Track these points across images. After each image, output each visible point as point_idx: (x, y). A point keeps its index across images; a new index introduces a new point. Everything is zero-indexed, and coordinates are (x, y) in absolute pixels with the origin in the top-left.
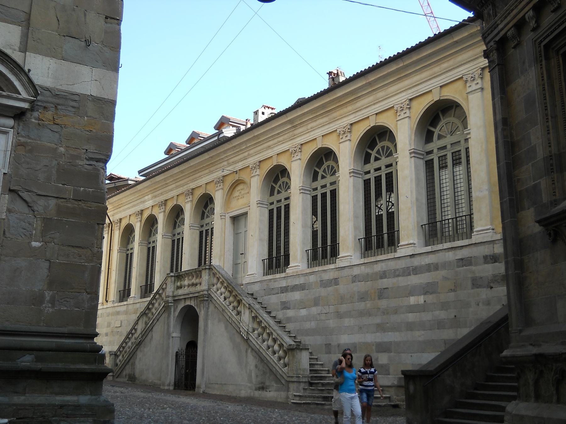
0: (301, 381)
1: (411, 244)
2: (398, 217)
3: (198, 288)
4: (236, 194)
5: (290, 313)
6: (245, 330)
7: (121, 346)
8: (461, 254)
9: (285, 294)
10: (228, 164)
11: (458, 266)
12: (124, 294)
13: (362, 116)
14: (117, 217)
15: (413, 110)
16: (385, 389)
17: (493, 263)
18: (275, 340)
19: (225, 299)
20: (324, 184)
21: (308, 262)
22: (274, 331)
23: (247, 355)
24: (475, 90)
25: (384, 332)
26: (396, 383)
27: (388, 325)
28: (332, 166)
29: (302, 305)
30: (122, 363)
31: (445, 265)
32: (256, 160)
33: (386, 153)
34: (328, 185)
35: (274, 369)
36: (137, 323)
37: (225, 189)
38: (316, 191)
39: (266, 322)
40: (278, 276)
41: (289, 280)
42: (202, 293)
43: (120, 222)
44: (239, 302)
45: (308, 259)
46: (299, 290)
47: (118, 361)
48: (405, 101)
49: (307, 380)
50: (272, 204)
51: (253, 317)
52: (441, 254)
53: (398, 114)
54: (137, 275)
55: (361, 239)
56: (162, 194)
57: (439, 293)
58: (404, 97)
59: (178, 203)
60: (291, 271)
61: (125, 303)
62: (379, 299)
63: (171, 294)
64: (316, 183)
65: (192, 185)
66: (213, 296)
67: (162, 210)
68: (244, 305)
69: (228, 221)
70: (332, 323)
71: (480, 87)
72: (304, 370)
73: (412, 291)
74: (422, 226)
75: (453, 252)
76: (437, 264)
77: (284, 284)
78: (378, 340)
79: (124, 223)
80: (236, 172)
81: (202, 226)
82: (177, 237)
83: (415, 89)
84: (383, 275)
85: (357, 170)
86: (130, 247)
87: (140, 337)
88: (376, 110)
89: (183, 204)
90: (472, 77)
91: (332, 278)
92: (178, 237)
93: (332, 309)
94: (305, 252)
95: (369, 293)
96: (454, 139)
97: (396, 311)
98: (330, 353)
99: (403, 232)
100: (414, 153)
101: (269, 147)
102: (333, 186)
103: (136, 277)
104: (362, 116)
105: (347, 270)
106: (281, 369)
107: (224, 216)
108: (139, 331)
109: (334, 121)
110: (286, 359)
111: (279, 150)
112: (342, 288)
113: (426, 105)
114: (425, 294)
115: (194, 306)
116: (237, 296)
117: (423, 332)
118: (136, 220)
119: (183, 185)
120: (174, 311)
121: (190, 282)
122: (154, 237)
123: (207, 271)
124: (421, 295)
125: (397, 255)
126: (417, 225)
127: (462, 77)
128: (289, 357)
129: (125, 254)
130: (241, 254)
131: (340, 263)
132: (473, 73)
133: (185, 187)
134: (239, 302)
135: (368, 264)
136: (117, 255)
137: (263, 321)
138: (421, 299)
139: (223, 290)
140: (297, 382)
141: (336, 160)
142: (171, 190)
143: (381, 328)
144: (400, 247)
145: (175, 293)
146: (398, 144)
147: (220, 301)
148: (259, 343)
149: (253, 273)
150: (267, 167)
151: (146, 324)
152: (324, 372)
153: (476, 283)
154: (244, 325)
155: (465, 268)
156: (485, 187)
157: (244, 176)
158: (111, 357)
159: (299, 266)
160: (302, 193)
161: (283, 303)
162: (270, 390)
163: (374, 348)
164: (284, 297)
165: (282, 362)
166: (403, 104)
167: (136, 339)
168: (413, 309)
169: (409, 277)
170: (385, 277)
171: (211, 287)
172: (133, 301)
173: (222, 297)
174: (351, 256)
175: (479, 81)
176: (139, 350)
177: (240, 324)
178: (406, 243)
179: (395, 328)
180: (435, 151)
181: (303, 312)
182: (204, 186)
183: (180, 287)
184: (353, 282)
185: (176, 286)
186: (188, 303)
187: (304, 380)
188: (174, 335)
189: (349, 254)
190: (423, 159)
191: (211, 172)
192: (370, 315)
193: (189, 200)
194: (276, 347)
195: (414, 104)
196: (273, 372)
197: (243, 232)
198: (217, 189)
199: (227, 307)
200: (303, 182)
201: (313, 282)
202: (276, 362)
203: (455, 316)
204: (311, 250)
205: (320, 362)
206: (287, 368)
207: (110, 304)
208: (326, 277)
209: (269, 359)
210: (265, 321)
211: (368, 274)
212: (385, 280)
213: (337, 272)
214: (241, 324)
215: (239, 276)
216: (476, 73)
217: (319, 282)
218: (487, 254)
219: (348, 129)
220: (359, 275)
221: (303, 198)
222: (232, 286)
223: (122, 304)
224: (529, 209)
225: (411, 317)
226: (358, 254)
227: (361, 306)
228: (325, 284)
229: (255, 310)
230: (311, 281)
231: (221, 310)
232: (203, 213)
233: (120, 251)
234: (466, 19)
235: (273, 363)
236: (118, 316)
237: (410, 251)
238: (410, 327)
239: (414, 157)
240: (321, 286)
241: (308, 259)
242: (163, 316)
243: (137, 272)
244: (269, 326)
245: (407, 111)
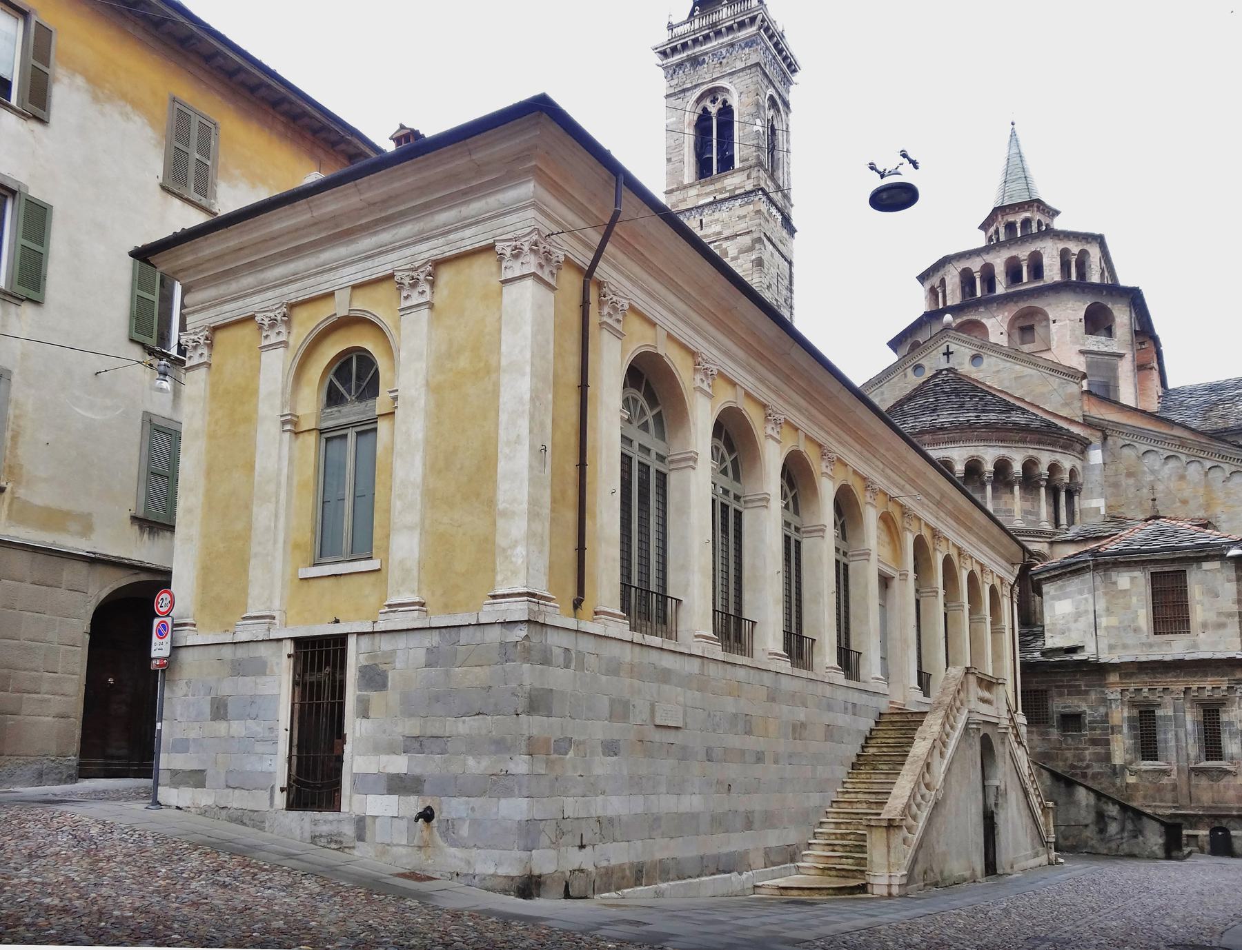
23: (1006, 786)
33: (358, 387)
90: (516, 248)
166: (199, 336)
195: (301, 315)
219: (282, 314)
234: (427, 135)
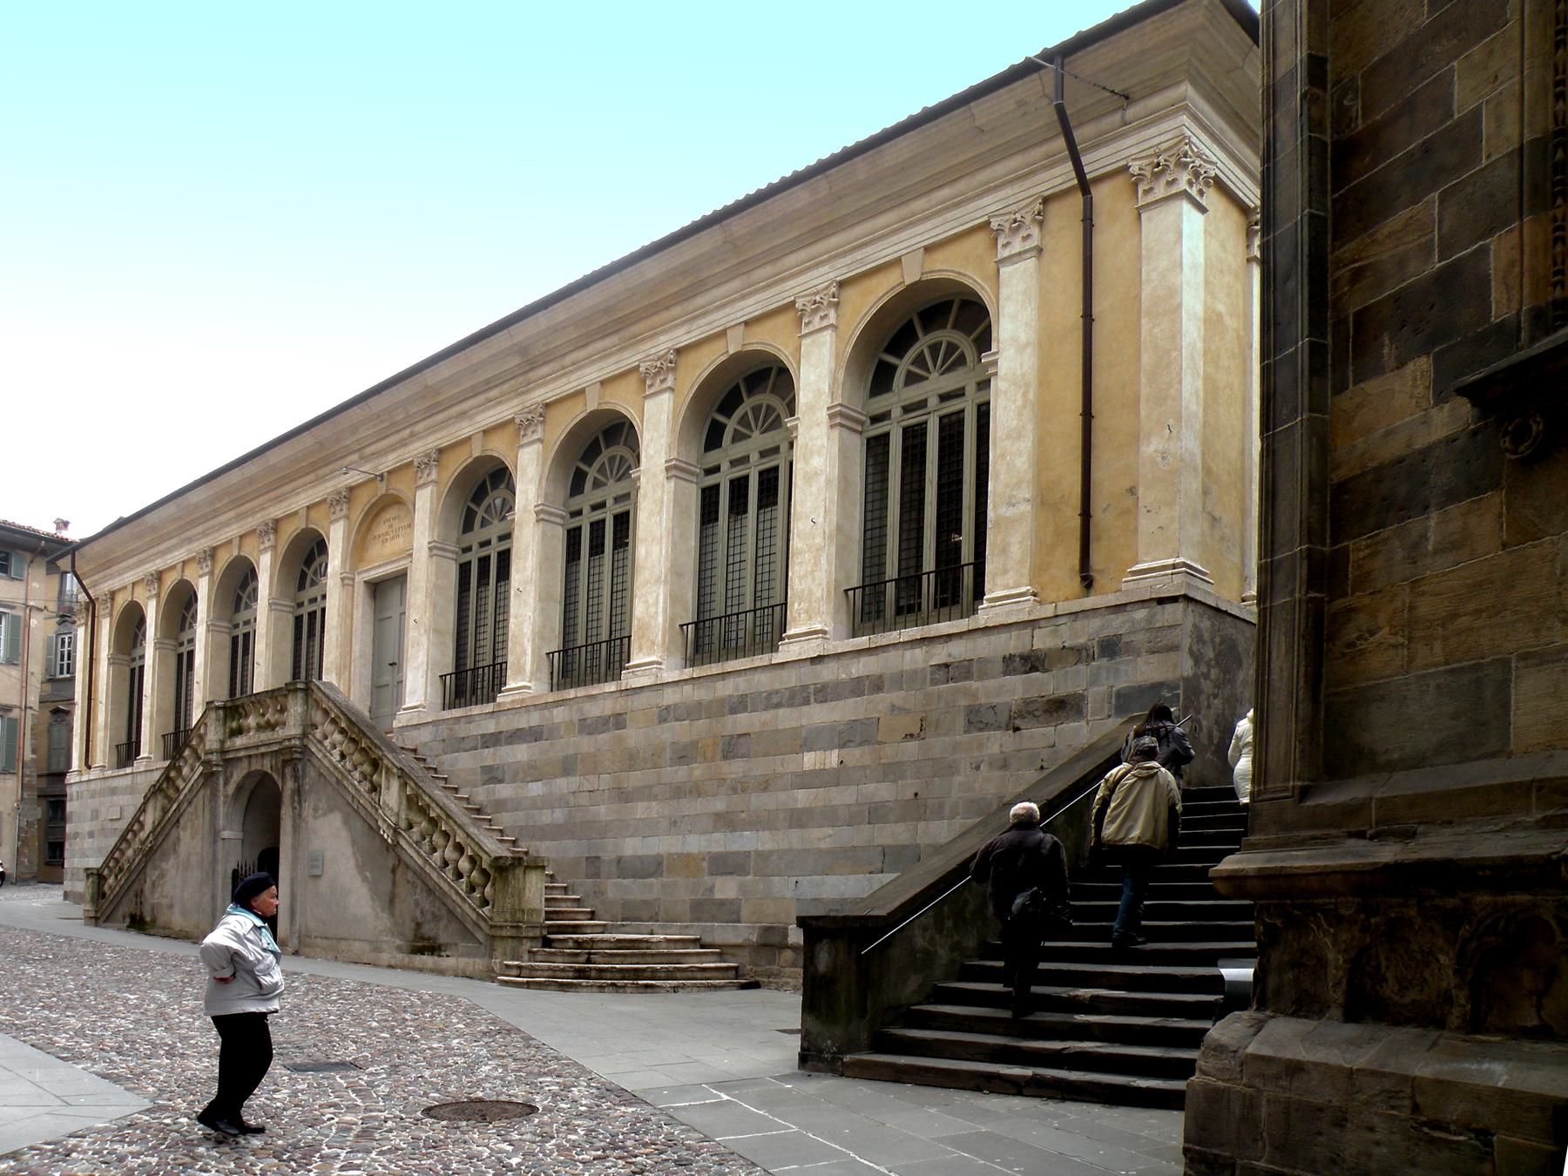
0: (524, 935)
1: (815, 632)
2: (784, 569)
3: (280, 733)
4: (381, 528)
5: (504, 791)
6: (389, 825)
7: (111, 855)
8: (941, 654)
9: (492, 750)
10: (362, 458)
11: (934, 682)
12: (128, 751)
13: (706, 328)
14: (107, 587)
15: (847, 309)
16: (725, 950)
17: (1026, 672)
18: (460, 849)
19: (343, 756)
20: (599, 500)
21: (552, 679)
22: (460, 826)
24: (1020, 254)
25: (734, 829)
26: (754, 938)
27: (743, 815)
28: (622, 457)
29: (533, 772)
30: (115, 892)
31: (901, 680)
32: (429, 446)
34: (610, 503)
35: (459, 910)
36: (144, 811)
37: (353, 517)
38: (577, 518)
39: (441, 808)
40: (476, 710)
41: (503, 719)
42: (287, 743)
43: (113, 599)
44: (376, 764)
45: (552, 673)
46: (525, 741)
47: (106, 888)
48: (827, 288)
49: (538, 934)
50: (467, 550)
51: (409, 798)
52: (892, 655)
53: (805, 320)
54: (152, 712)
55: (687, 625)
56: (205, 534)
57: (880, 743)
58: (824, 276)
59: (242, 554)
60: (509, 699)
61: (128, 770)
62: (725, 757)
63: (216, 746)
64: (579, 498)
65: (277, 512)
66: (313, 749)
67: (206, 570)
68: (388, 770)
69: (360, 591)
70: (603, 812)
71: (1036, 243)
72: (532, 911)
73: (809, 740)
74: (846, 591)
75: (924, 648)
76: (880, 677)
77: (490, 727)
78: (716, 849)
79: (121, 600)
80: (382, 476)
81: (300, 605)
82: (240, 632)
83: (858, 255)
84: (739, 704)
85: (686, 463)
86: (137, 653)
87: (151, 839)
88: (746, 311)
89: (255, 555)
90: (1015, 221)
91: (608, 712)
92: (246, 631)
93: (605, 781)
94: (545, 656)
95: (700, 745)
96: (950, 382)
97: (765, 786)
98: (597, 875)
99: (796, 605)
100: (840, 418)
101: (463, 415)
102: (622, 504)
103: (151, 717)
104: (706, 328)
105: (644, 696)
106: (475, 910)
107: (348, 578)
108: (148, 827)
109: (631, 345)
110: (488, 889)
111: (489, 421)
112: (634, 736)
113: (884, 295)
114: (842, 746)
115: (270, 772)
116: (370, 748)
117: (830, 831)
118: (148, 594)
119: (253, 512)
120: (226, 783)
121: (262, 721)
122: (192, 630)
123: (300, 695)
124: (832, 749)
125: (777, 658)
126: (836, 588)
127: (988, 223)
128: (493, 885)
129: (128, 671)
130: (391, 665)
131: (630, 680)
132: (1019, 210)
133: (259, 515)
134: (376, 764)
135: (702, 680)
136: (108, 670)
137: (433, 805)
138: (833, 758)
139: (337, 737)
140: (512, 937)
141: (634, 446)
142: (227, 524)
143: (724, 821)
144: (787, 641)
145: (228, 744)
146: (801, 393)
147: (330, 761)
148: (422, 853)
149: (417, 704)
150: (457, 463)
151: (165, 811)
152: (581, 917)
153: (977, 719)
154: (389, 813)
155: (951, 684)
156: (1026, 492)
157: (400, 486)
158: (91, 879)
159: (529, 688)
160: (542, 519)
161: (487, 769)
162: (448, 953)
163: (705, 864)
164: (489, 756)
165: (477, 895)
167: (143, 843)
168: (807, 780)
169: (805, 708)
170: (745, 710)
171: (309, 730)
172: (146, 766)
173: (336, 753)
174: (660, 664)
175: (1035, 231)
176: (150, 866)
177: (377, 810)
178: (804, 629)
179: (758, 823)
180: (896, 413)
181: (536, 789)
182: (303, 512)
183: (239, 731)
184: (662, 720)
185: (227, 730)
186: (256, 766)
187: (531, 934)
188: (226, 834)
189: (653, 658)
190: (861, 433)
191: (321, 480)
192: (699, 794)
193: (267, 544)
194: (464, 864)
196: (457, 918)
197: (396, 617)
198: (335, 517)
199: (346, 773)
200: (546, 494)
201: (560, 723)
202: (463, 894)
203: (916, 795)
204: (559, 652)
205: (573, 894)
206: (489, 907)
207: (94, 774)
208: (594, 710)
209: (446, 888)
210: (437, 804)
211: (699, 703)
212: (742, 716)
213: (621, 701)
214: (380, 811)
215: (386, 710)
216: (1027, 210)
217: (577, 722)
218: (1012, 652)
220: (676, 705)
221: (544, 534)
222: (359, 729)
223: (122, 772)
224: (1401, 364)
225: (803, 798)
226: (678, 659)
227: (680, 773)
228: (589, 727)
229: (413, 781)
230: (556, 721)
231: (333, 780)
232: (303, 576)
233: (112, 661)
235: (454, 897)
236: (115, 798)
237: (812, 648)
238: (799, 819)
239: (841, 425)
240: (580, 732)
241: (552, 673)
242: (202, 792)
243: (152, 706)
244: (448, 816)
245: (832, 313)
